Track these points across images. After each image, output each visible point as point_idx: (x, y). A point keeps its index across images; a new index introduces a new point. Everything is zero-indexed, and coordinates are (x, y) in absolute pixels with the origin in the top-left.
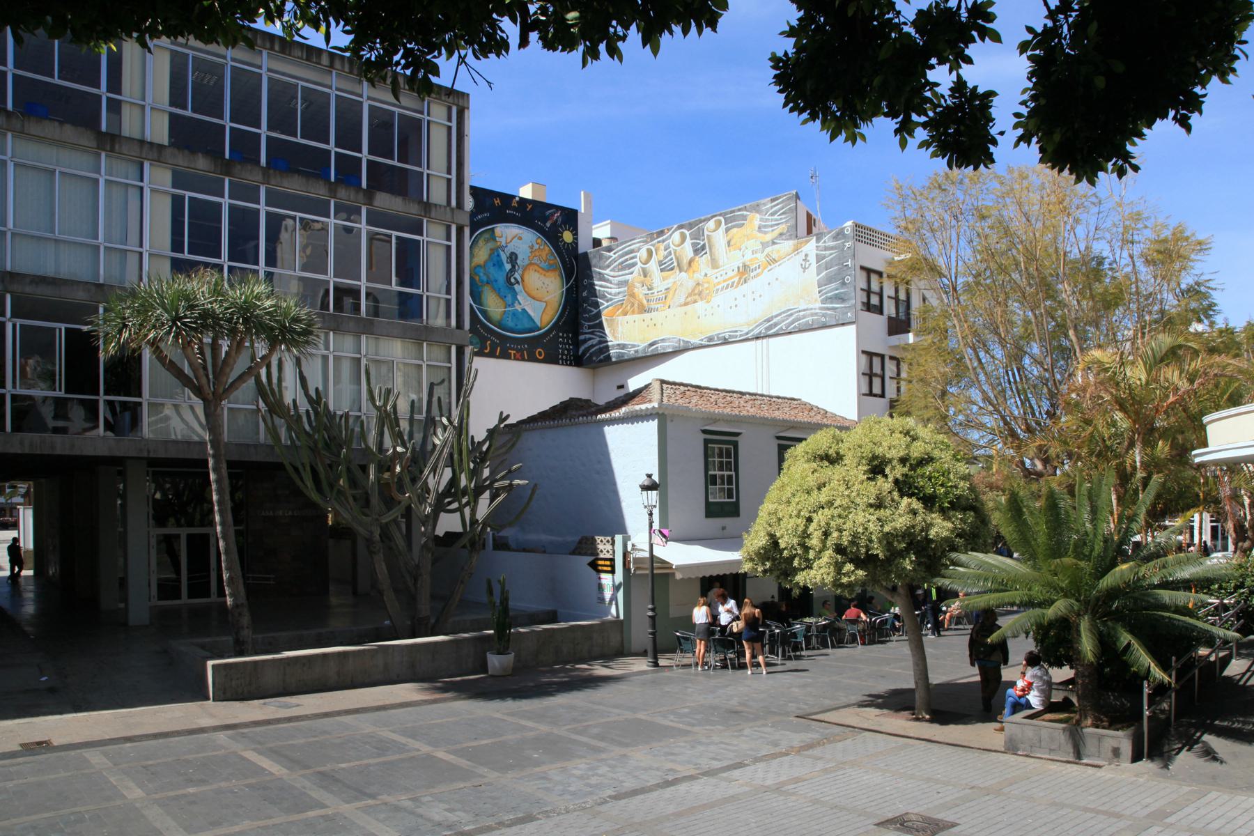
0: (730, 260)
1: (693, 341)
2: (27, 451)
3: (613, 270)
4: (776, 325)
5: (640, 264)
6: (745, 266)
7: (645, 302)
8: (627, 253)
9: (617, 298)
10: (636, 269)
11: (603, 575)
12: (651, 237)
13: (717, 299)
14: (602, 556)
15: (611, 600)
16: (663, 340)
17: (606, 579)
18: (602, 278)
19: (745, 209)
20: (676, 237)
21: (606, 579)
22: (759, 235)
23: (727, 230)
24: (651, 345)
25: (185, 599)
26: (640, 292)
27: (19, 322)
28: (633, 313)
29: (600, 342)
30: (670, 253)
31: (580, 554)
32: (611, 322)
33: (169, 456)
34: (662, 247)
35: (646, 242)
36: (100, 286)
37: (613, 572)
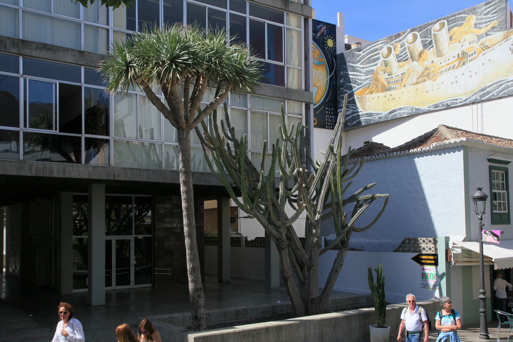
0: (451, 50)
1: (422, 108)
2: (34, 175)
3: (362, 64)
4: (488, 93)
5: (382, 58)
6: (463, 53)
7: (386, 84)
8: (372, 52)
9: (365, 83)
10: (379, 62)
11: (426, 267)
12: (391, 39)
13: (440, 79)
14: (424, 252)
15: (435, 286)
16: (400, 109)
17: (430, 270)
18: (354, 69)
19: (464, 12)
20: (410, 37)
21: (430, 270)
22: (475, 30)
23: (449, 29)
24: (391, 112)
25: (132, 285)
26: (383, 77)
27: (28, 77)
28: (377, 91)
29: (353, 113)
30: (405, 49)
31: (403, 251)
32: (361, 99)
33: (127, 179)
34: (399, 45)
35: (386, 43)
36: (81, 53)
37: (436, 264)
